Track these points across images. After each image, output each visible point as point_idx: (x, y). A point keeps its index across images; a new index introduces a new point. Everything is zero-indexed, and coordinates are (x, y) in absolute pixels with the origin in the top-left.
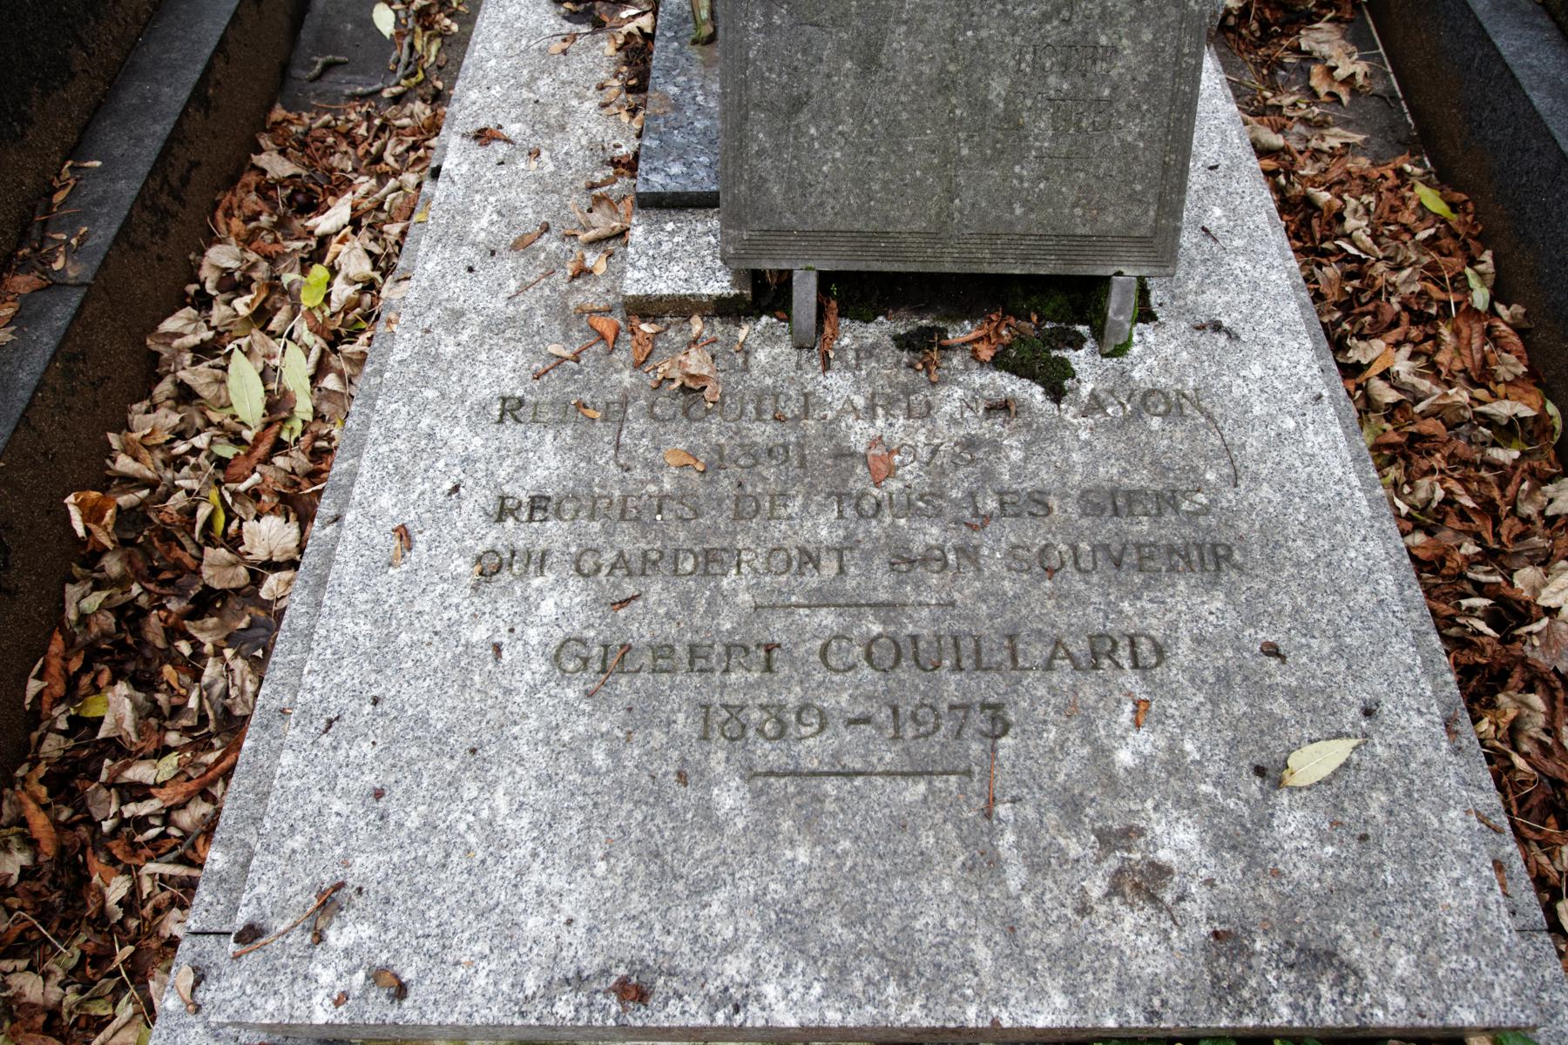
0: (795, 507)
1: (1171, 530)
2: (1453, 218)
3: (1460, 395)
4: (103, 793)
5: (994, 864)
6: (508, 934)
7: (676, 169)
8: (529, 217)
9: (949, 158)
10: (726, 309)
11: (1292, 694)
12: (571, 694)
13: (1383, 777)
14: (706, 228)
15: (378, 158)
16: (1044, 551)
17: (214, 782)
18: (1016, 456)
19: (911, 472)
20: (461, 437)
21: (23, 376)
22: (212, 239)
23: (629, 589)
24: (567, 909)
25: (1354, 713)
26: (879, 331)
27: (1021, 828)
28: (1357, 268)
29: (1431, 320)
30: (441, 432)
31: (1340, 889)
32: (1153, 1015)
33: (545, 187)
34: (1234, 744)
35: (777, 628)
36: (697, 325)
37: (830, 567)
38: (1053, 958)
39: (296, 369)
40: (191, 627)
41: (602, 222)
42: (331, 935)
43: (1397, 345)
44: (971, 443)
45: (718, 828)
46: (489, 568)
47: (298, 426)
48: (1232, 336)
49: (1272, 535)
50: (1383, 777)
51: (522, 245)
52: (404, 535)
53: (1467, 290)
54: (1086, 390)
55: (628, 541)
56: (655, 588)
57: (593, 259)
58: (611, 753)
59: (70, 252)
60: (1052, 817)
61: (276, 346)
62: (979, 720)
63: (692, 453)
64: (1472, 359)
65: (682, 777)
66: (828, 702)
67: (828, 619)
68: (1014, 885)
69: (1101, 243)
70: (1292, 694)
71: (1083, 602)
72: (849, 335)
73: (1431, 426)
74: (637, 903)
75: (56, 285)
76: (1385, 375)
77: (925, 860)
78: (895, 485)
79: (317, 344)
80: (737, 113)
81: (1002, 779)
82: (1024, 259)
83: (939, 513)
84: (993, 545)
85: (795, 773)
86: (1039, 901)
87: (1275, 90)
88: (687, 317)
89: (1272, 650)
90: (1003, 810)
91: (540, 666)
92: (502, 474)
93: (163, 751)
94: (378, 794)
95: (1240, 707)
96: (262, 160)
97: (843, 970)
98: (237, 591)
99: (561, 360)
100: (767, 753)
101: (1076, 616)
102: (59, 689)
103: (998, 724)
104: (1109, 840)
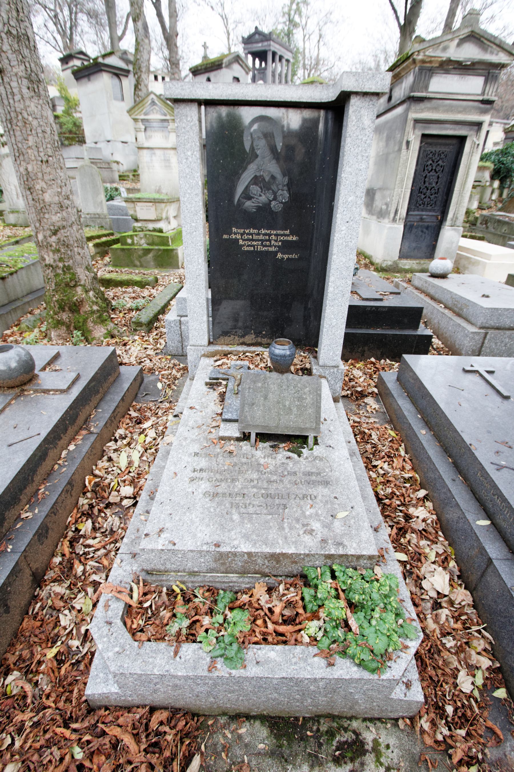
0: (250, 472)
1: (319, 478)
2: (397, 437)
3: (397, 472)
4: (80, 546)
5: (283, 529)
6: (194, 536)
7: (230, 415)
8: (200, 422)
9: (279, 414)
10: (238, 439)
11: (339, 505)
12: (207, 500)
13: (354, 518)
14: (236, 425)
15: (157, 414)
16: (295, 481)
17: (107, 545)
18: (291, 466)
19: (271, 467)
20: (186, 458)
21: (84, 450)
22: (118, 428)
23: (218, 484)
24: (205, 533)
25: (350, 508)
26: (267, 444)
27: (288, 523)
28: (375, 446)
29: (392, 457)
30: (183, 457)
31: (345, 534)
32: (310, 551)
33: (203, 418)
34: (328, 512)
35: (245, 491)
36: (232, 442)
37: (256, 482)
38: (293, 543)
39: (135, 456)
40: (105, 510)
41: (214, 424)
42: (162, 535)
43: (384, 462)
44: (283, 463)
45: (234, 521)
46: (192, 480)
47: (134, 468)
48: (333, 448)
49: (337, 480)
50: (354, 518)
51: (199, 427)
52: (175, 473)
53: (400, 451)
54: (305, 456)
55: (218, 476)
56: (223, 484)
57: (212, 430)
58: (215, 509)
59: (95, 427)
60: (294, 522)
61: (131, 451)
62: (282, 507)
63: (231, 463)
64: (400, 466)
65: (227, 514)
66: (255, 503)
67: (255, 490)
68: (286, 531)
69: (306, 429)
70: (339, 505)
71: (301, 489)
72: (261, 445)
73: (391, 479)
74: (218, 532)
75: (91, 433)
76: (381, 468)
77: (271, 527)
78: (268, 470)
79: (142, 450)
80: (243, 406)
81: (285, 515)
82: (293, 432)
83: (276, 474)
84: (286, 480)
85: (248, 514)
86: (291, 534)
87: (359, 410)
88: (230, 441)
89: (336, 498)
90: (285, 520)
91: (201, 496)
92: (194, 465)
93: (95, 538)
94: (171, 514)
95: (329, 506)
96: (129, 413)
97: (255, 543)
98: (116, 503)
99: (206, 447)
100: (242, 510)
101: (301, 491)
102: (74, 521)
103: (285, 507)
104: (304, 525)
